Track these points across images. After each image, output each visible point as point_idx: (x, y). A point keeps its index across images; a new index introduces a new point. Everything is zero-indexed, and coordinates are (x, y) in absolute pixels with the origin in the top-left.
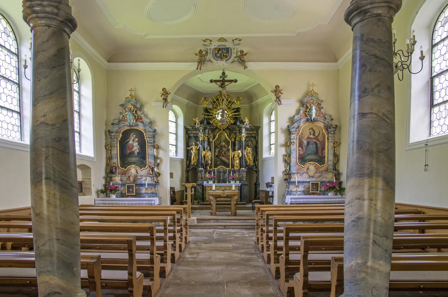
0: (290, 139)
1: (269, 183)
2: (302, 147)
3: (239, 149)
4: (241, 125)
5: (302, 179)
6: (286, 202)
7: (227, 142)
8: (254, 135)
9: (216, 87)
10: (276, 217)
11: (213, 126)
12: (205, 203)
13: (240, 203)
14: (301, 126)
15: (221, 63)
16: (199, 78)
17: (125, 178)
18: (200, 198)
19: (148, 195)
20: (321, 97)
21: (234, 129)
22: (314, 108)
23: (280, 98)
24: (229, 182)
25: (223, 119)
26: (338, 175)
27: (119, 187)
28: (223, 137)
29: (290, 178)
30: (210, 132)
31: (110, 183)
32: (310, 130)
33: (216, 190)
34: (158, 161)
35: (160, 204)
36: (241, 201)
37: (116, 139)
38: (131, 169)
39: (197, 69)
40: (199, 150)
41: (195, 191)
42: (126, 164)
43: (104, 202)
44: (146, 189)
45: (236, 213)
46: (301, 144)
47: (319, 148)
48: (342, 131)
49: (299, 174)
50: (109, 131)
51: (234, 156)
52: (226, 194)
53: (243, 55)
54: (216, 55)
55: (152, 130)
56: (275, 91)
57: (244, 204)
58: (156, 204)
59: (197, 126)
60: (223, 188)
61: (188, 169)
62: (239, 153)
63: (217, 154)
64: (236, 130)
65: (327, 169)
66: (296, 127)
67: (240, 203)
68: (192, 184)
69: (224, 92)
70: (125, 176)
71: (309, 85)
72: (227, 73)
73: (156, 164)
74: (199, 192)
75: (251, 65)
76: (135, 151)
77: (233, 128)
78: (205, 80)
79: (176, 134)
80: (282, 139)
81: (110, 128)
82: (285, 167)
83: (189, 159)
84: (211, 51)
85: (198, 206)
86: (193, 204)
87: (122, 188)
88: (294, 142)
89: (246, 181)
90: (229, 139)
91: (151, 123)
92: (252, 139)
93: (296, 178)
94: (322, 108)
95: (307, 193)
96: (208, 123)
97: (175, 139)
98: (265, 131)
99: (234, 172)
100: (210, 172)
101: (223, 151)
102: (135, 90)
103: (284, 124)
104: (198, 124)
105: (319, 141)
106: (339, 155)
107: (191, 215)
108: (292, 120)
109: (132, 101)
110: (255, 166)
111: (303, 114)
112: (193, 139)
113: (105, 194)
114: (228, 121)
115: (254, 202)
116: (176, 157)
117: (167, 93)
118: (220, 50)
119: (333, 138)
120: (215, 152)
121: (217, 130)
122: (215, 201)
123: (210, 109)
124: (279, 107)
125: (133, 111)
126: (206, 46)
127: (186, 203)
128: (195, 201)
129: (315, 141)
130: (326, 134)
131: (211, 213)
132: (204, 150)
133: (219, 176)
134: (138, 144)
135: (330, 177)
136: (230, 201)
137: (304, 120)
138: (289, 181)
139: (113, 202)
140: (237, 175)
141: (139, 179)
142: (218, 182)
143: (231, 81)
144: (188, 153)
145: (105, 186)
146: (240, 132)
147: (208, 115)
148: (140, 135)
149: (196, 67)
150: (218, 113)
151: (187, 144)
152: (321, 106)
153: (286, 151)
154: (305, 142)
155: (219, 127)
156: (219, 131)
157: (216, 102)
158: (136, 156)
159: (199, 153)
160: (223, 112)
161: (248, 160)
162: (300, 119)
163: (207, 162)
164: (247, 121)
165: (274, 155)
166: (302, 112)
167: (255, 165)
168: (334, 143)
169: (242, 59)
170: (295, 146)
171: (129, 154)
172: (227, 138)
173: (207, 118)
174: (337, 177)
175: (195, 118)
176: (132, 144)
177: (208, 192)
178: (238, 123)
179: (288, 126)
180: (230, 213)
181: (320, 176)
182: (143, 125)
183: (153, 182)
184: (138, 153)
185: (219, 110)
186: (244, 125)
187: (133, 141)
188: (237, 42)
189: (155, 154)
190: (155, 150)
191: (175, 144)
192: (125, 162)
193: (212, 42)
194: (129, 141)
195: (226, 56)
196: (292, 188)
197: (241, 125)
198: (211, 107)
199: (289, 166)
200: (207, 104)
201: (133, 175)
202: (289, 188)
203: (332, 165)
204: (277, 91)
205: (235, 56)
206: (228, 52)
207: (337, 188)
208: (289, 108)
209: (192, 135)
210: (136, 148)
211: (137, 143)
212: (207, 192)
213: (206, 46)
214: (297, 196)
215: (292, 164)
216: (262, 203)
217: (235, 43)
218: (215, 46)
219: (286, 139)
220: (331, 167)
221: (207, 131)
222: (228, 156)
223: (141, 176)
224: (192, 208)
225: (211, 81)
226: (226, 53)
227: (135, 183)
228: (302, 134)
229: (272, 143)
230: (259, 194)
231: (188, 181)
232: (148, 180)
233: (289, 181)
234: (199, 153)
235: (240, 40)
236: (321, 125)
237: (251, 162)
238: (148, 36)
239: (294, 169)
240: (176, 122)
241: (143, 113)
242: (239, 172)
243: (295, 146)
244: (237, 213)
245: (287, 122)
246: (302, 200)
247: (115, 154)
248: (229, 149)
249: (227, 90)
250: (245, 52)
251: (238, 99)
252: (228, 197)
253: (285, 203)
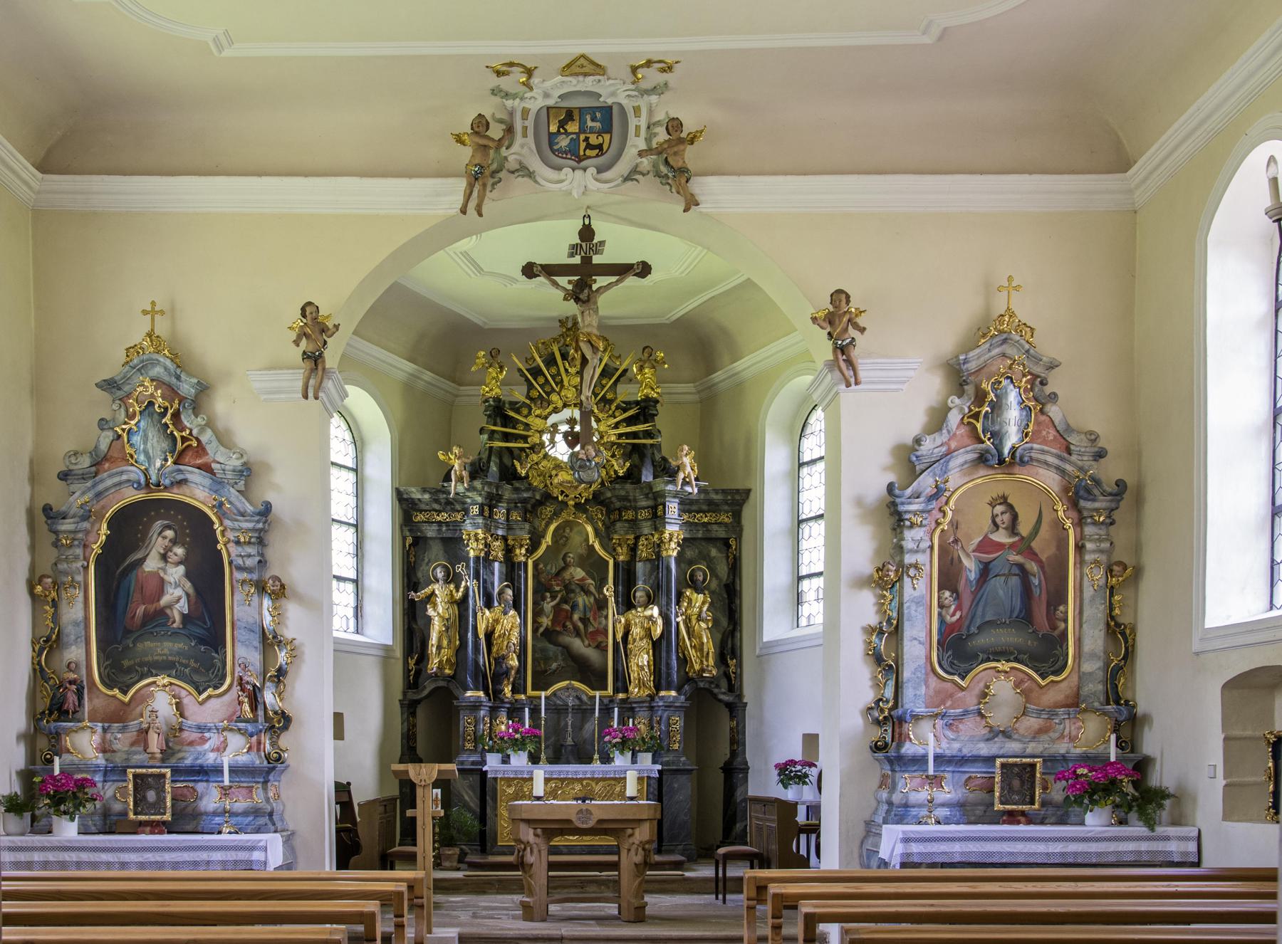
0: (900, 549)
2: (954, 591)
3: (650, 601)
5: (956, 745)
6: (884, 853)
7: (595, 567)
9: (549, 300)
10: (857, 931)
11: (530, 488)
13: (658, 858)
14: (951, 485)
15: (577, 183)
16: (465, 254)
17: (121, 741)
18: (474, 839)
19: (234, 820)
20: (1047, 346)
22: (1012, 397)
23: (855, 353)
24: (606, 759)
26: (1129, 724)
27: (94, 784)
28: (576, 539)
29: (900, 738)
30: (515, 516)
31: (51, 761)
32: (992, 505)
33: (552, 794)
34: (282, 657)
35: (288, 866)
37: (79, 551)
38: (152, 695)
39: (464, 211)
40: (462, 604)
42: (130, 670)
43: (22, 857)
44: (225, 791)
46: (949, 578)
47: (1036, 592)
48: (1150, 509)
49: (939, 723)
50: (47, 509)
51: (627, 633)
52: (598, 815)
53: (681, 141)
54: (551, 144)
55: (249, 508)
56: (831, 319)
57: (677, 865)
58: (271, 867)
59: (454, 487)
60: (578, 787)
61: (412, 696)
62: (650, 618)
64: (636, 509)
65: (1078, 695)
66: (930, 490)
67: (658, 858)
68: (437, 767)
69: (589, 324)
70: (123, 729)
71: (989, 289)
72: (602, 230)
73: (272, 672)
74: (466, 806)
75: (708, 188)
76: (170, 606)
78: (495, 265)
79: (358, 527)
80: (861, 549)
81: (54, 494)
82: (877, 685)
83: (417, 644)
84: (530, 123)
85: (459, 875)
87: (109, 790)
88: (916, 566)
89: (685, 752)
90: (602, 553)
91: (247, 473)
92: (714, 552)
93: (926, 740)
94: (1053, 397)
95: (979, 811)
96: (508, 475)
97: (352, 549)
98: (773, 511)
99: (628, 709)
101: (574, 607)
102: (172, 312)
103: (872, 476)
104: (460, 479)
105: (1039, 562)
106: (1133, 631)
108: (909, 460)
109: (155, 363)
110: (724, 683)
111: (963, 431)
112: (436, 550)
113: (28, 815)
115: (728, 857)
116: (796, 633)
117: (323, 330)
118: (570, 115)
119: (1105, 545)
120: (538, 613)
121: (548, 510)
122: (544, 848)
123: (516, 406)
124: (848, 397)
125: (164, 414)
126: (507, 95)
127: (410, 859)
129: (1019, 559)
130: (1068, 524)
131: (525, 906)
132: (489, 604)
133: (556, 730)
134: (188, 575)
135: (1089, 735)
136: (616, 851)
137: (964, 457)
138: (892, 753)
139: (66, 856)
140: (640, 724)
141: (191, 743)
142: (555, 759)
143: (621, 270)
144: (412, 617)
145: (26, 776)
146: (655, 516)
147: (507, 437)
148: (197, 531)
149: (459, 199)
150: (555, 426)
151: (410, 578)
152: (1048, 390)
153: (881, 609)
154: (970, 565)
155: (556, 493)
156: (556, 514)
158: (175, 634)
159: (463, 617)
161: (692, 652)
162: (949, 453)
163: (500, 660)
164: (687, 463)
165: (821, 629)
166: (954, 418)
167: (727, 675)
168: (1109, 570)
169: (673, 163)
170: (921, 585)
171: (144, 624)
172: (597, 546)
174: (1126, 733)
175: (448, 450)
176: (155, 574)
178: (647, 476)
179: (890, 488)
180: (612, 909)
181: (1042, 731)
182: (207, 482)
183: (257, 761)
184: (186, 618)
185: (556, 411)
186: (674, 482)
187: (164, 557)
188: (652, 77)
189: (267, 620)
190: (267, 602)
191: (353, 575)
192: (126, 663)
193: (535, 80)
194: (143, 560)
195: (600, 147)
196: (911, 788)
198: (519, 395)
199: (891, 683)
200: (504, 383)
201: (160, 722)
202: (893, 788)
203: (1100, 674)
204: (839, 319)
205: (643, 146)
206: (607, 128)
207: (1129, 789)
208: (897, 396)
209: (431, 532)
210: (178, 592)
211: (181, 569)
213: (507, 95)
214: (932, 828)
215: (907, 674)
216: (765, 863)
217: (644, 85)
218: (546, 95)
219: (878, 552)
220: (1095, 688)
221: (500, 513)
222: (597, 632)
223: (201, 728)
225: (530, 271)
226: (599, 133)
227: (173, 761)
228: (955, 525)
231: (410, 754)
232: (235, 751)
233: (892, 753)
234: (463, 617)
235: (668, 69)
236: (1049, 480)
237: (704, 660)
238: (231, 43)
239: (915, 698)
240: (356, 470)
241: (210, 424)
242: (651, 708)
243: (921, 585)
244: (648, 911)
245: (886, 469)
246: (957, 847)
247: (76, 624)
248: (606, 600)
250: (689, 126)
251: (647, 357)
252: (605, 832)
253: (874, 863)
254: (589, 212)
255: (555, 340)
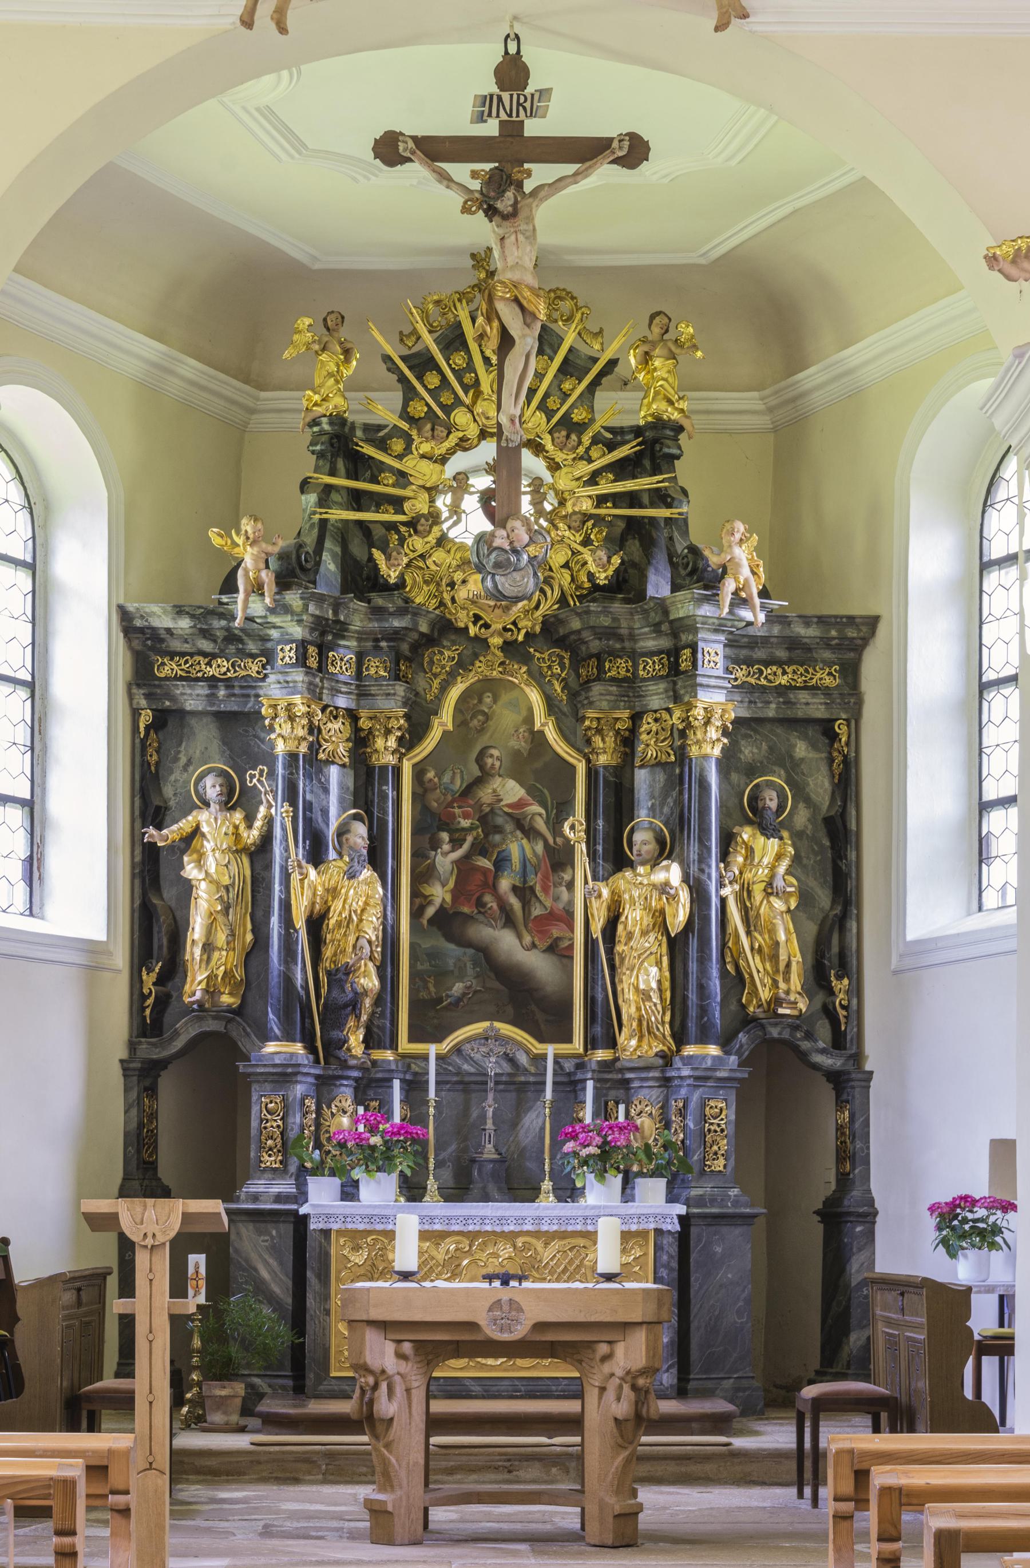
1: (968, 1201)
3: (664, 851)
4: (687, 606)
7: (548, 778)
8: (816, 708)
9: (431, 215)
11: (407, 608)
12: (316, 1407)
13: (668, 1407)
16: (268, 113)
21: (617, 642)
24: (568, 1192)
25: (501, 541)
30: (375, 667)
33: (428, 1269)
36: (681, 1392)
39: (248, 21)
40: (260, 853)
41: (220, 1282)
45: (631, 1515)
52: (534, 1313)
57: (719, 1423)
59: (245, 606)
60: (505, 1251)
61: (148, 1050)
63: (439, 894)
64: (634, 656)
67: (668, 1407)
69: (516, 263)
74: (261, 1289)
77: (609, 633)
83: (161, 939)
85: (240, 1442)
86: (197, 1422)
89: (739, 1176)
90: (561, 748)
92: (801, 749)
96: (362, 580)
97: (23, 735)
99: (616, 1083)
100: (370, 1087)
101: (501, 863)
104: (258, 589)
107: (172, 1541)
112: (204, 740)
114: (558, 558)
115: (823, 1406)
120: (422, 875)
121: (447, 656)
122: (418, 1384)
128: (220, 1390)
132: (316, 856)
133: (463, 1129)
142: (459, 1190)
143: (585, 151)
144: (152, 883)
146: (675, 670)
147: (357, 500)
150: (461, 480)
151: (149, 797)
155: (462, 619)
156: (463, 665)
157: (435, 368)
159: (260, 883)
160: (506, 466)
163: (340, 976)
164: (743, 561)
167: (829, 1012)
172: (551, 734)
173: (344, 532)
175: (230, 525)
177: (357, 1291)
178: (658, 585)
180: (567, 1517)
185: (464, 445)
186: (713, 599)
197: (687, 606)
198: (385, 410)
200: (353, 386)
212: (341, 1286)
221: (343, 660)
222: (552, 917)
224: (185, 1467)
225: (389, 149)
229: (991, 792)
230: (867, 1319)
231: (143, 1178)
234: (260, 883)
240: (31, 567)
242: (666, 1082)
249: (544, 238)
251: (660, 335)
254: (518, 29)
255: (462, 296)
